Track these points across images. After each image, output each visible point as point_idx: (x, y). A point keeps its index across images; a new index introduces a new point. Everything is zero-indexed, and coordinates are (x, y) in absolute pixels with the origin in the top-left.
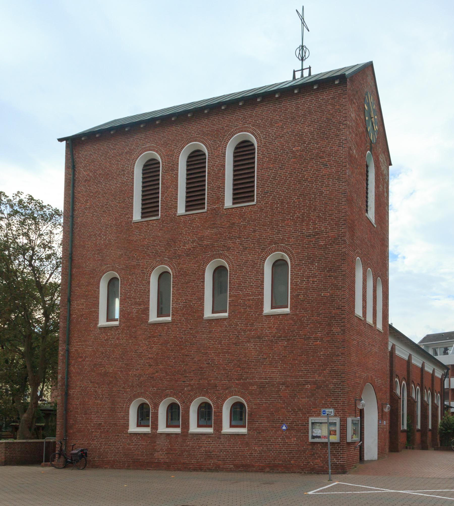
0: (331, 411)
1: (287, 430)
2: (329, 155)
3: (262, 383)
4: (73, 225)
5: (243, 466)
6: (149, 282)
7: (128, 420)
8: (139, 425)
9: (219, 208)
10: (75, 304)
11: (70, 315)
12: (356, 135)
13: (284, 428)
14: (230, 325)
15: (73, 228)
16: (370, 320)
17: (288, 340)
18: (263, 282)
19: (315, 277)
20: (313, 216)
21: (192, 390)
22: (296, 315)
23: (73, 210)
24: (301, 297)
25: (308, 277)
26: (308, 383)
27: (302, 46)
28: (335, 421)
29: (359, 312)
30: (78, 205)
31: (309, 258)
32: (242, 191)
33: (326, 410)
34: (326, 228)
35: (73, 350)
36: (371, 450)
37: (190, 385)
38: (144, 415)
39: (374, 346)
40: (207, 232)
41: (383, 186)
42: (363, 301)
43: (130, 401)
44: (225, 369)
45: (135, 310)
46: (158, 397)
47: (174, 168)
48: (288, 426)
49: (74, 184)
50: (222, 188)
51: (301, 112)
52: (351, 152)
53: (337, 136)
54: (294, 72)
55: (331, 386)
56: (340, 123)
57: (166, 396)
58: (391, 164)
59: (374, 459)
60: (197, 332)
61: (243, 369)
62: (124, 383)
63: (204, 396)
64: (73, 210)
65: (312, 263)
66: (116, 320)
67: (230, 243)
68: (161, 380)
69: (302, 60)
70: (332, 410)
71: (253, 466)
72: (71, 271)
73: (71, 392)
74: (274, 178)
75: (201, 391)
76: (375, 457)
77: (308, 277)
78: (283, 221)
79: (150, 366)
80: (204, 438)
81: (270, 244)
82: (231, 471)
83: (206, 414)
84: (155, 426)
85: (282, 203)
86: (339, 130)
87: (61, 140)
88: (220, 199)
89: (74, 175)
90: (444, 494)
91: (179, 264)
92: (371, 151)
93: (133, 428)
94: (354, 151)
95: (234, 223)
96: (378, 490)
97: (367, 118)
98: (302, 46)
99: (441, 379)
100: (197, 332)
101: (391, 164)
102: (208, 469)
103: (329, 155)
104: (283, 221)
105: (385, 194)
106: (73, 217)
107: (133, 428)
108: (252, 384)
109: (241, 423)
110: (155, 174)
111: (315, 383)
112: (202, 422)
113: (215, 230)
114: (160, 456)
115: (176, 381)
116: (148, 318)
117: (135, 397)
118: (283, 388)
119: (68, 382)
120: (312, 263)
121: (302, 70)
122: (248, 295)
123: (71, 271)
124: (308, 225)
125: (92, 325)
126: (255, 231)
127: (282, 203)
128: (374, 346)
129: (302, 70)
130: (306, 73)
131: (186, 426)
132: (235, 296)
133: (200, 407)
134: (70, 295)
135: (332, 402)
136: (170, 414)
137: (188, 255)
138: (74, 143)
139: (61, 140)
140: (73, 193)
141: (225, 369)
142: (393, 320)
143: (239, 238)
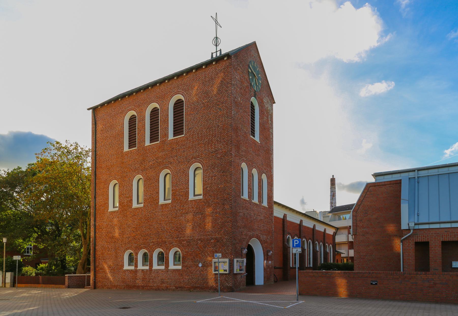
0: (220, 255)
2: (222, 103)
4: (96, 155)
5: (180, 287)
6: (132, 185)
8: (143, 265)
9: (166, 140)
10: (97, 199)
11: (95, 205)
12: (241, 89)
14: (172, 207)
15: (96, 157)
16: (256, 200)
17: (202, 214)
18: (188, 181)
19: (215, 176)
21: (154, 245)
22: (206, 199)
23: (96, 148)
24: (208, 189)
25: (212, 177)
26: (212, 239)
27: (216, 37)
29: (245, 196)
30: (98, 144)
31: (212, 165)
32: (178, 130)
34: (221, 147)
35: (97, 224)
36: (259, 279)
37: (153, 242)
38: (132, 259)
39: (259, 215)
40: (160, 154)
41: (267, 117)
42: (248, 189)
43: (124, 252)
44: (170, 232)
46: (138, 249)
47: (144, 119)
49: (96, 133)
50: (167, 129)
51: (207, 79)
52: (236, 100)
53: (226, 91)
54: (212, 53)
55: (225, 240)
56: (228, 83)
57: (141, 248)
58: (274, 103)
60: (156, 212)
61: (179, 232)
62: (122, 242)
63: (160, 248)
64: (96, 148)
65: (214, 168)
66: (117, 207)
67: (171, 160)
68: (139, 239)
69: (216, 46)
70: (220, 254)
71: (185, 288)
72: (95, 181)
73: (97, 248)
75: (159, 245)
76: (262, 283)
77: (212, 177)
78: (199, 144)
80: (160, 272)
81: (192, 159)
82: (174, 290)
83: (162, 258)
84: (136, 266)
85: (198, 134)
86: (227, 87)
87: (89, 109)
88: (166, 135)
89: (96, 128)
90: (277, 304)
91: (147, 173)
92: (255, 97)
93: (126, 267)
94: (239, 99)
95: (173, 148)
96: (231, 300)
97: (251, 77)
98: (216, 37)
99: (333, 235)
100: (156, 212)
101: (274, 103)
102: (163, 289)
103: (222, 103)
104: (199, 144)
105: (270, 122)
106: (96, 151)
107: (126, 267)
108: (183, 241)
109: (179, 263)
110: (133, 123)
111: (216, 239)
112: (160, 263)
113: (164, 153)
114: (139, 282)
115: (146, 240)
116: (132, 206)
117: (127, 249)
118: (199, 242)
119: (95, 242)
120: (214, 168)
121: (217, 52)
123: (95, 181)
124: (211, 145)
125: (106, 210)
126: (184, 151)
127: (198, 134)
128: (259, 215)
129: (217, 52)
130: (218, 55)
131: (151, 265)
133: (159, 254)
134: (95, 194)
137: (151, 168)
138: (95, 109)
139: (89, 109)
140: (96, 137)
141: (170, 232)
142: (276, 198)
143: (176, 156)
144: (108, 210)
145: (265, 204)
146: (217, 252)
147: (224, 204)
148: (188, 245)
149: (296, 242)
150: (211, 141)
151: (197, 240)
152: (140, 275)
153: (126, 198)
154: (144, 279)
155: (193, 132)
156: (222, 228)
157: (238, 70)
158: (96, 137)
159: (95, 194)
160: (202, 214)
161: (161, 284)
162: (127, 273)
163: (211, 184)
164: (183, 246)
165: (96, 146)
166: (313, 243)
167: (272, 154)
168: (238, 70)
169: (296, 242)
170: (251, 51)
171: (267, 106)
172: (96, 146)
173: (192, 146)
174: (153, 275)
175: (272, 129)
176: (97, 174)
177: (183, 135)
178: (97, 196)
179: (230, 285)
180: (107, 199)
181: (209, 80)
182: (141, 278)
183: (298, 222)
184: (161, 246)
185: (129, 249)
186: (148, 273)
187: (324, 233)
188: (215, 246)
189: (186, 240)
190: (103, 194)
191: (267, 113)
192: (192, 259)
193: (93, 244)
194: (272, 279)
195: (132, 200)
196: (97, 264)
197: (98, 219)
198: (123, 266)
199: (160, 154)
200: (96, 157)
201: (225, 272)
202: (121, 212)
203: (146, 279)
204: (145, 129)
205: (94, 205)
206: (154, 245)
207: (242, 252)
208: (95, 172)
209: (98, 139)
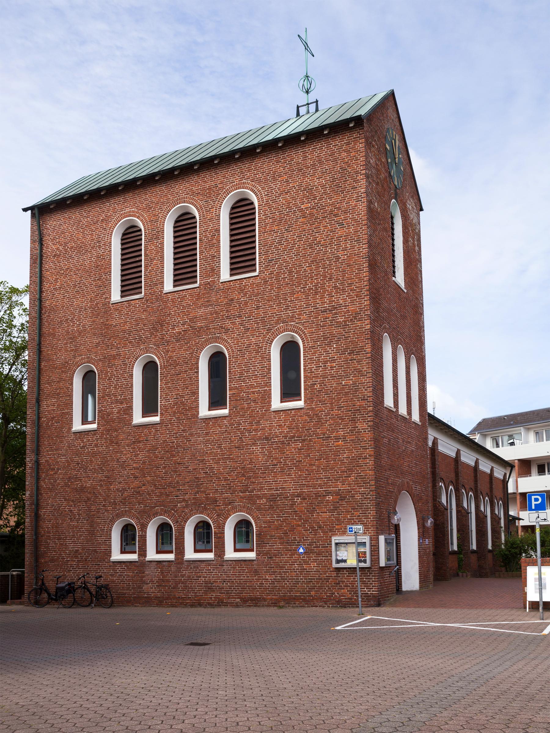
1: (305, 553)
2: (345, 212)
3: (273, 495)
5: (252, 599)
7: (110, 546)
9: (213, 282)
10: (44, 404)
11: (39, 418)
12: (377, 184)
13: (301, 550)
14: (232, 424)
15: (40, 313)
17: (304, 440)
18: (269, 369)
20: (329, 287)
21: (187, 506)
23: (41, 292)
24: (317, 387)
25: (325, 362)
26: (328, 493)
28: (364, 541)
30: (46, 285)
31: (325, 339)
33: (353, 527)
35: (43, 461)
36: (411, 579)
37: (184, 500)
38: (129, 537)
40: (201, 312)
41: (413, 238)
43: (113, 522)
45: (115, 410)
46: (145, 516)
48: (306, 548)
50: (216, 257)
53: (354, 188)
55: (358, 497)
57: (156, 514)
58: (422, 210)
59: (414, 589)
60: (191, 435)
61: (249, 478)
63: (201, 513)
64: (41, 292)
65: (329, 345)
68: (149, 494)
70: (360, 527)
71: (265, 600)
73: (42, 512)
74: (280, 243)
75: (198, 506)
79: (136, 477)
81: (277, 323)
83: (205, 535)
84: (143, 552)
85: (290, 272)
87: (25, 210)
88: (215, 271)
91: (168, 351)
94: (376, 204)
97: (389, 160)
100: (191, 435)
101: (422, 210)
103: (345, 212)
104: (292, 293)
105: (417, 248)
108: (259, 497)
111: (337, 493)
112: (200, 546)
113: (210, 309)
114: (150, 589)
115: (168, 496)
119: (38, 500)
120: (329, 345)
122: (252, 386)
123: (40, 365)
124: (322, 297)
125: (65, 430)
126: (258, 308)
132: (236, 388)
133: (197, 527)
134: (39, 394)
135: (359, 516)
136: (160, 537)
138: (41, 212)
139: (25, 210)
141: (226, 479)
143: (240, 317)
144: (70, 428)
145: (416, 417)
146: (355, 523)
147: (354, 420)
148: (271, 507)
149: (536, 500)
150: (323, 287)
151: (293, 495)
152: (151, 573)
153: (116, 403)
154: (162, 583)
155: (280, 268)
156: (351, 470)
157: (373, 146)
158: (41, 271)
159: (39, 394)
160: (304, 440)
161: (206, 593)
162: (119, 569)
163: (324, 376)
164: (259, 509)
165: (41, 289)
166: (457, 490)
167: (422, 314)
168: (373, 146)
169: (536, 500)
170: (388, 109)
171: (412, 216)
172: (41, 289)
173: (277, 296)
174: (186, 573)
175: (421, 262)
176: (44, 349)
177: (256, 273)
178: (43, 397)
179: (374, 591)
180: (70, 405)
181: (314, 165)
182: (155, 579)
183: (453, 454)
184: (205, 509)
185: (123, 516)
186: (173, 569)
187: (476, 468)
188: (336, 508)
189: (264, 496)
190: (58, 394)
191: (413, 230)
192: (280, 538)
193: (31, 504)
194: (431, 577)
195: (131, 408)
196: (42, 549)
197: (44, 449)
198: (109, 553)
199: (201, 312)
200: (40, 313)
201: (362, 565)
202: (102, 434)
203: (168, 581)
204: (162, 257)
205: (35, 417)
206: (187, 506)
207: (389, 521)
208: (40, 344)
209: (46, 274)
